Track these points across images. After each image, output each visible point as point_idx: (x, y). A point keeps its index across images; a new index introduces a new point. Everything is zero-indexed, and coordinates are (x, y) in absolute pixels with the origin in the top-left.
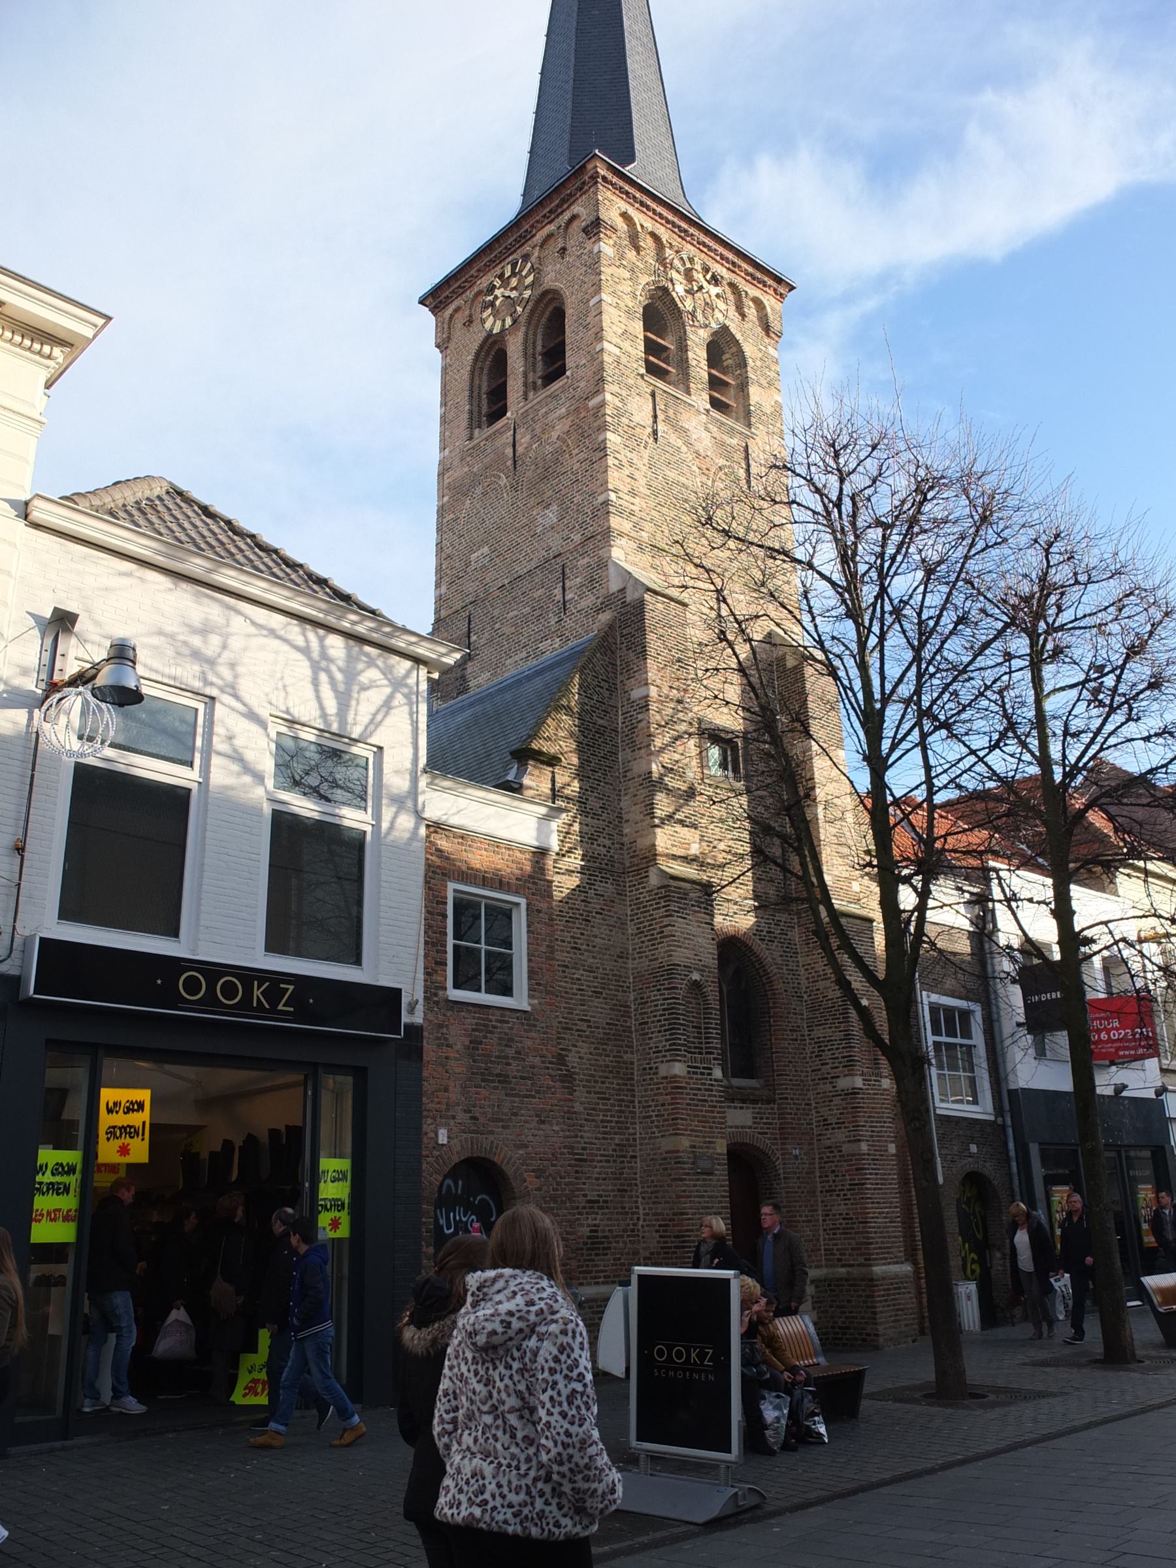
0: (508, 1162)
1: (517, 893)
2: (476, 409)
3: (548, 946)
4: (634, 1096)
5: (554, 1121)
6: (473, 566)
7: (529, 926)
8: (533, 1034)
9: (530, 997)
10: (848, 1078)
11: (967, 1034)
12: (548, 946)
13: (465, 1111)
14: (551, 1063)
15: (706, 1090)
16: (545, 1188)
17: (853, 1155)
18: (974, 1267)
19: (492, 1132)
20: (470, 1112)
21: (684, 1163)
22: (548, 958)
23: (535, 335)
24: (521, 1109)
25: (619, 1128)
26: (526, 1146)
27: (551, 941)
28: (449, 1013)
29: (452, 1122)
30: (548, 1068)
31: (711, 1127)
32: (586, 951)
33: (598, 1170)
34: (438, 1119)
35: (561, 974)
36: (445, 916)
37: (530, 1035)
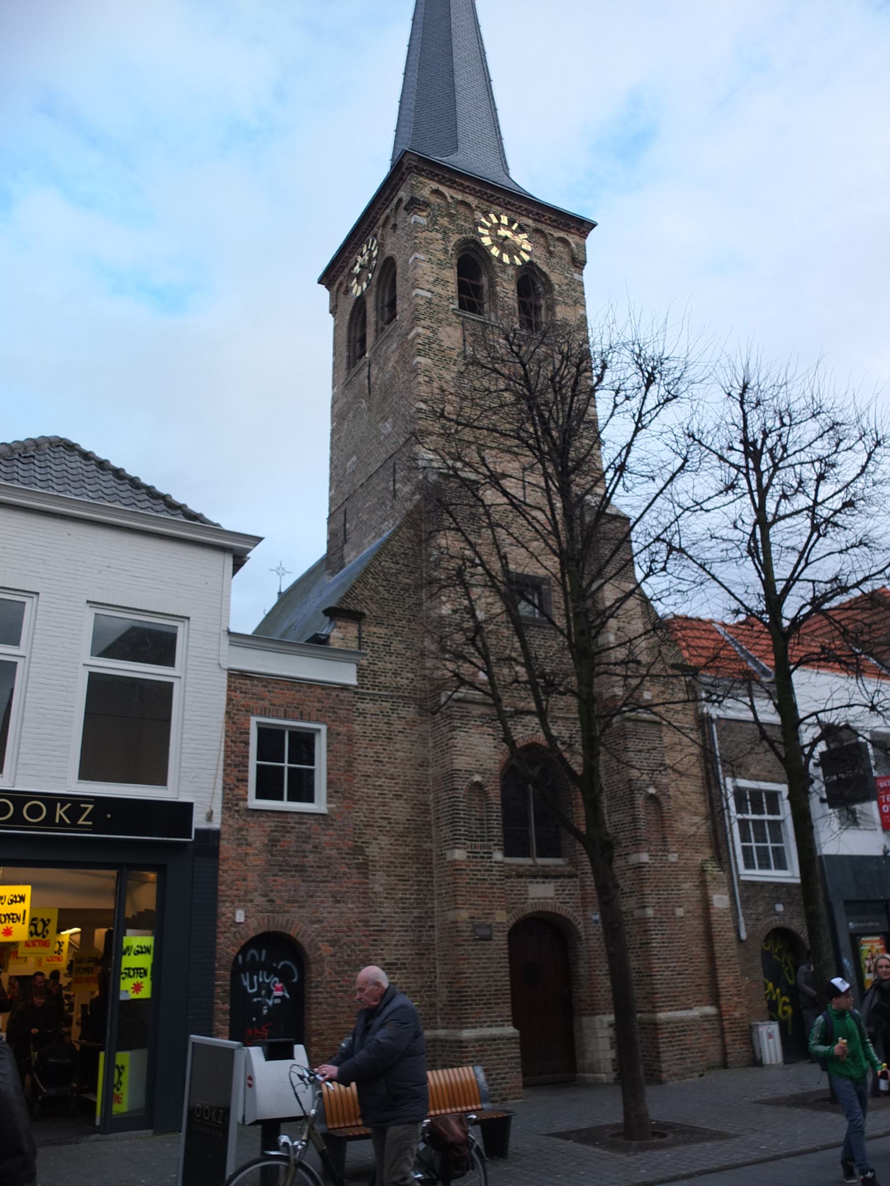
0: (303, 935)
1: (317, 721)
2: (352, 354)
3: (346, 761)
4: (432, 877)
5: (350, 901)
6: (349, 471)
7: (328, 746)
8: (330, 832)
9: (329, 802)
10: (636, 855)
11: (775, 810)
12: (346, 761)
13: (263, 896)
14: (346, 854)
15: (486, 871)
16: (339, 955)
17: (642, 919)
18: (785, 1008)
19: (288, 912)
20: (267, 896)
21: (463, 931)
22: (346, 771)
23: (383, 292)
24: (317, 891)
25: (418, 904)
26: (320, 922)
27: (349, 757)
28: (249, 819)
29: (249, 905)
30: (344, 858)
31: (491, 901)
32: (387, 762)
33: (396, 938)
34: (237, 903)
35: (363, 782)
36: (247, 743)
37: (327, 832)
